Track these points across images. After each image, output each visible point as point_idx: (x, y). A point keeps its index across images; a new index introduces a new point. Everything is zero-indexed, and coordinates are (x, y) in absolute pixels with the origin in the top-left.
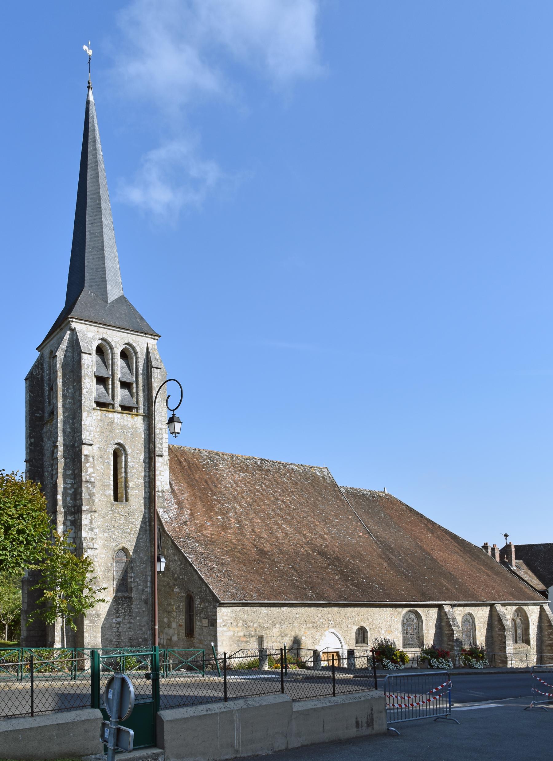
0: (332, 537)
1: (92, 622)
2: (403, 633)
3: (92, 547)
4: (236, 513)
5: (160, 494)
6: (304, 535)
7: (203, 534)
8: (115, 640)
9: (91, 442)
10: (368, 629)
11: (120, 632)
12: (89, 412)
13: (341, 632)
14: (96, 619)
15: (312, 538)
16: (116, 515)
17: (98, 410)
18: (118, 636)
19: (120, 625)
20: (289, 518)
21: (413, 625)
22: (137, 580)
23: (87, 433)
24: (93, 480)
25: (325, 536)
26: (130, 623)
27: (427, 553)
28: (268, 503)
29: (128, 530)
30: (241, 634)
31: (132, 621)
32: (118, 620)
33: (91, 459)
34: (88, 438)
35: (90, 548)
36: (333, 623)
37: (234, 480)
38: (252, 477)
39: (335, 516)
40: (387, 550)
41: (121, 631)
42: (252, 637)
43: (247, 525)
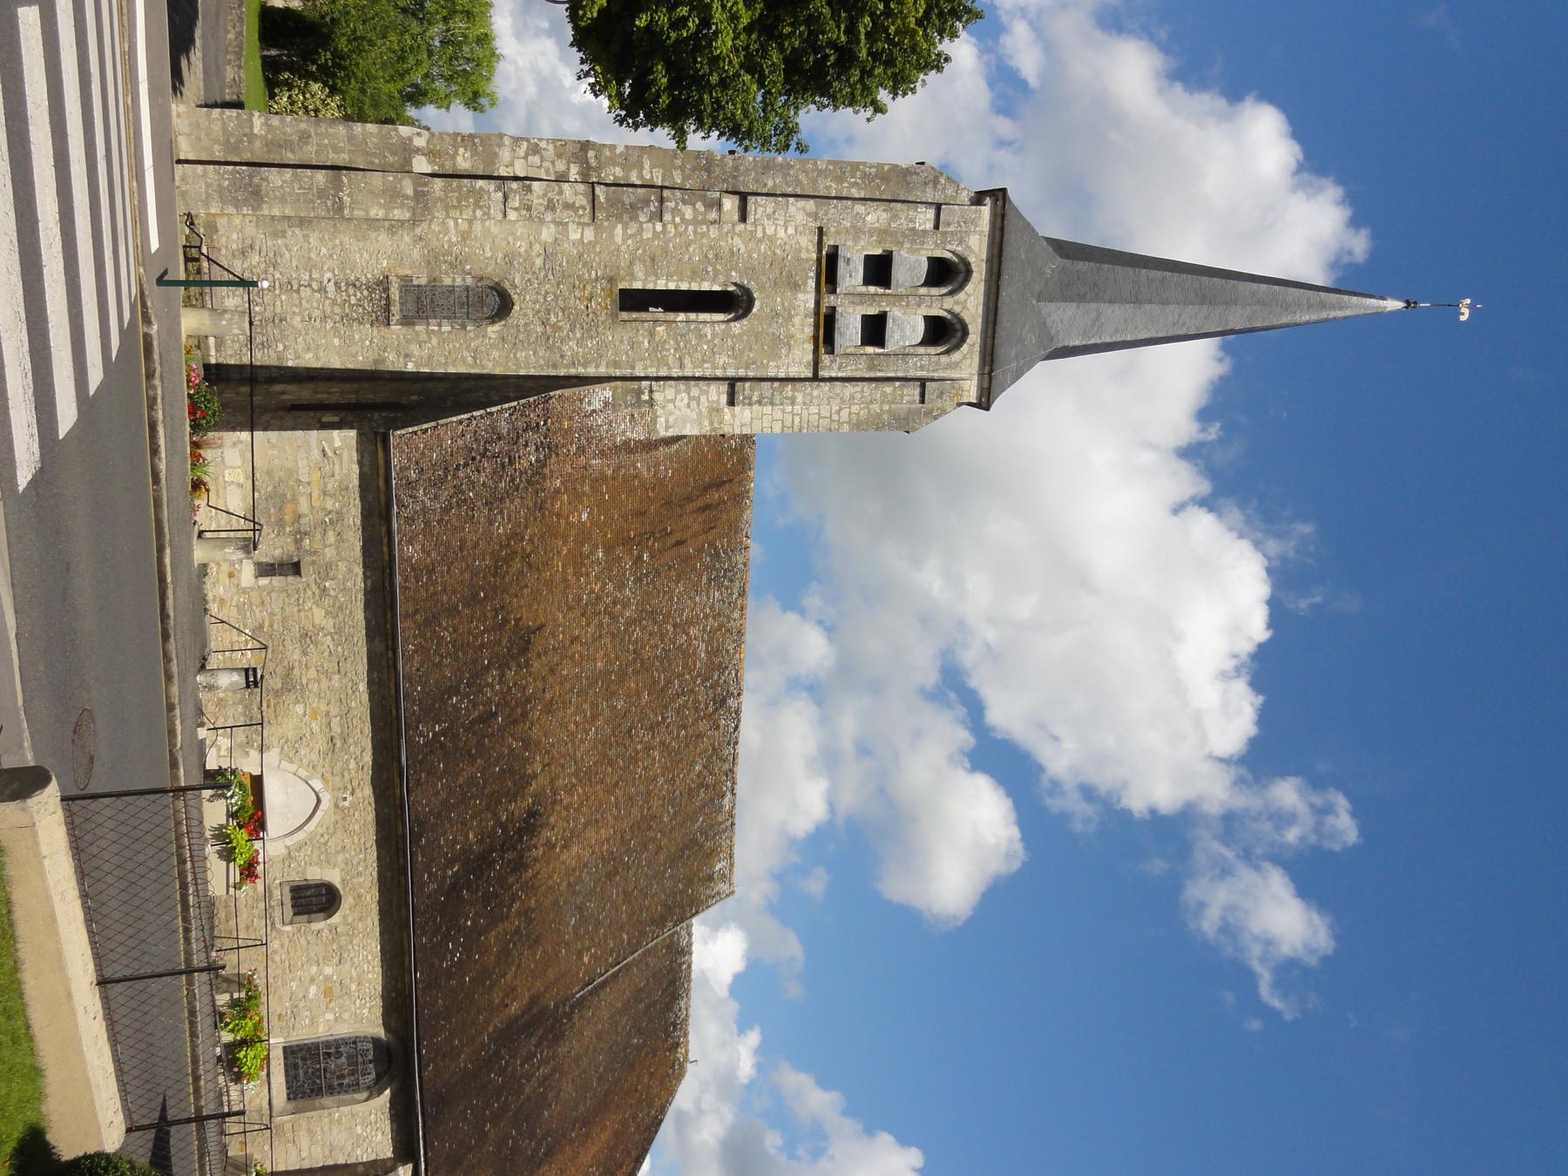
0: (574, 870)
1: (322, 194)
2: (328, 1044)
3: (511, 204)
4: (615, 603)
5: (645, 397)
6: (574, 786)
7: (557, 491)
8: (277, 275)
9: (751, 219)
10: (336, 919)
11: (298, 291)
12: (816, 217)
13: (320, 831)
14: (329, 203)
15: (567, 808)
16: (589, 288)
17: (820, 250)
18: (288, 287)
19: (319, 291)
20: (612, 753)
21: (353, 1073)
22: (434, 341)
23: (769, 210)
24: (667, 217)
25: (575, 849)
26: (325, 318)
27: (550, 1153)
28: (643, 702)
29: (553, 319)
30: (304, 507)
31: (329, 325)
32: (331, 287)
33: (713, 215)
34: (760, 210)
35: (506, 198)
36: (347, 804)
37: (689, 623)
38: (699, 675)
39: (625, 893)
40: (545, 1023)
41: (303, 294)
42: (296, 542)
43: (588, 625)
